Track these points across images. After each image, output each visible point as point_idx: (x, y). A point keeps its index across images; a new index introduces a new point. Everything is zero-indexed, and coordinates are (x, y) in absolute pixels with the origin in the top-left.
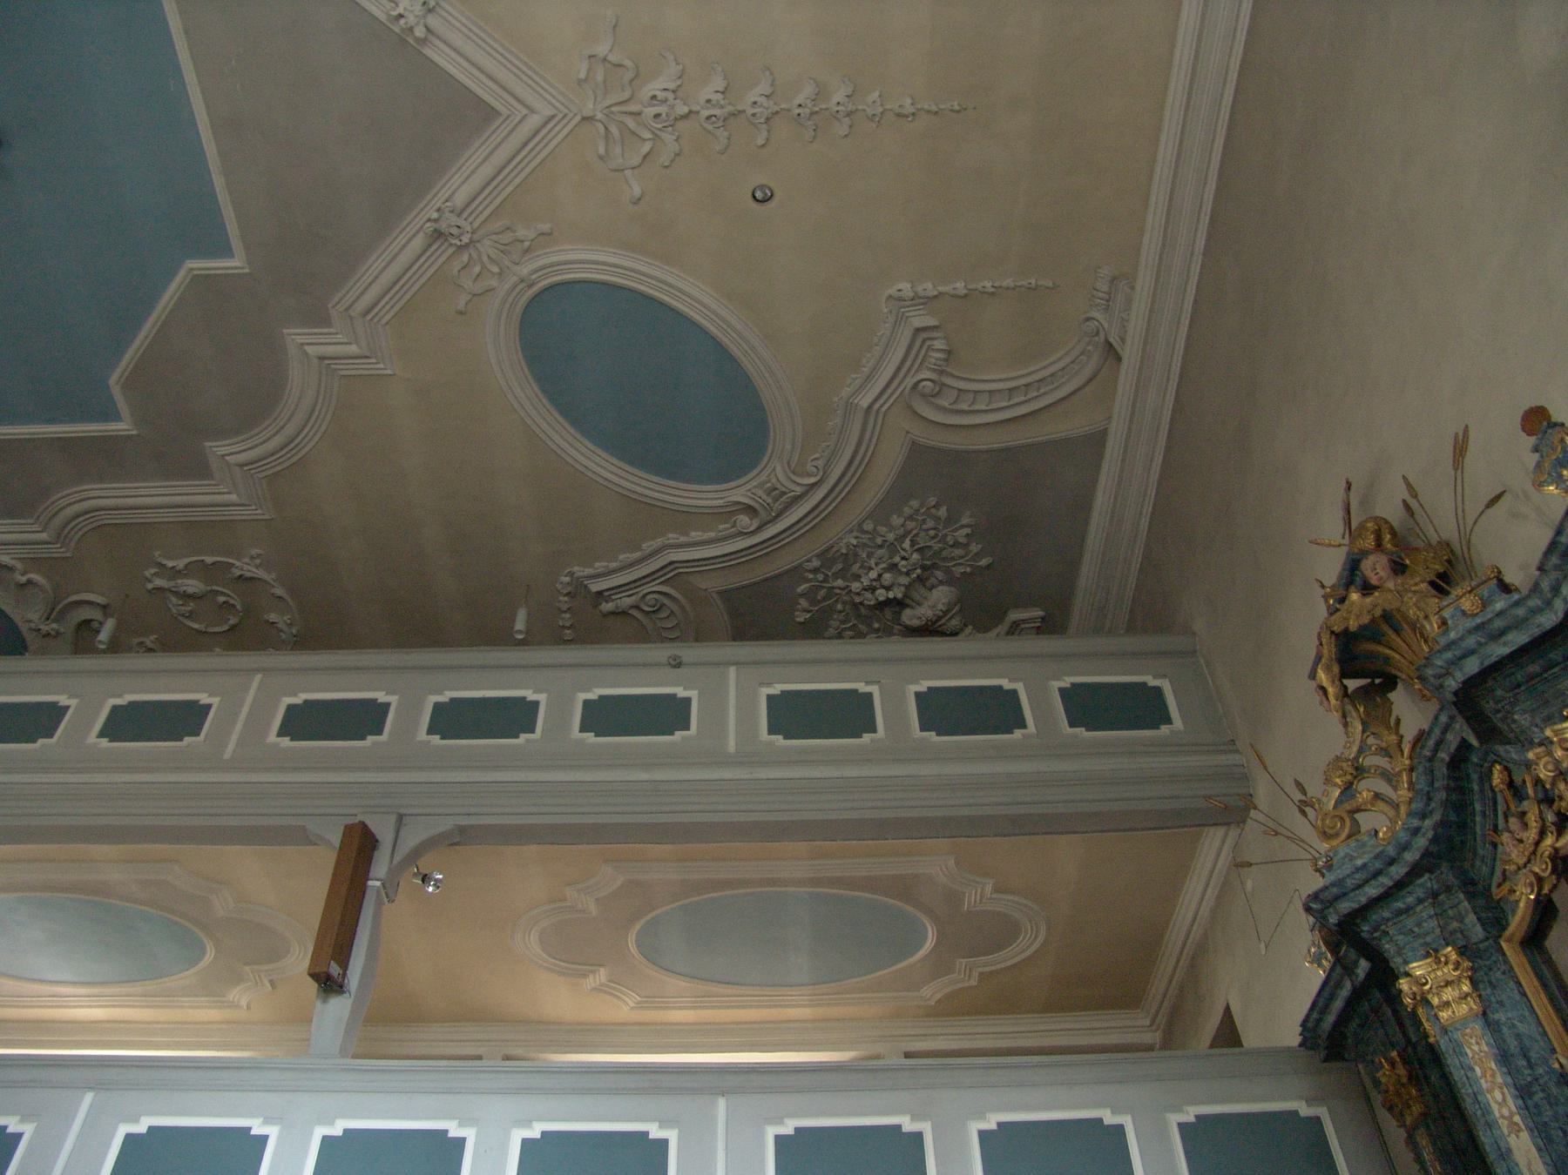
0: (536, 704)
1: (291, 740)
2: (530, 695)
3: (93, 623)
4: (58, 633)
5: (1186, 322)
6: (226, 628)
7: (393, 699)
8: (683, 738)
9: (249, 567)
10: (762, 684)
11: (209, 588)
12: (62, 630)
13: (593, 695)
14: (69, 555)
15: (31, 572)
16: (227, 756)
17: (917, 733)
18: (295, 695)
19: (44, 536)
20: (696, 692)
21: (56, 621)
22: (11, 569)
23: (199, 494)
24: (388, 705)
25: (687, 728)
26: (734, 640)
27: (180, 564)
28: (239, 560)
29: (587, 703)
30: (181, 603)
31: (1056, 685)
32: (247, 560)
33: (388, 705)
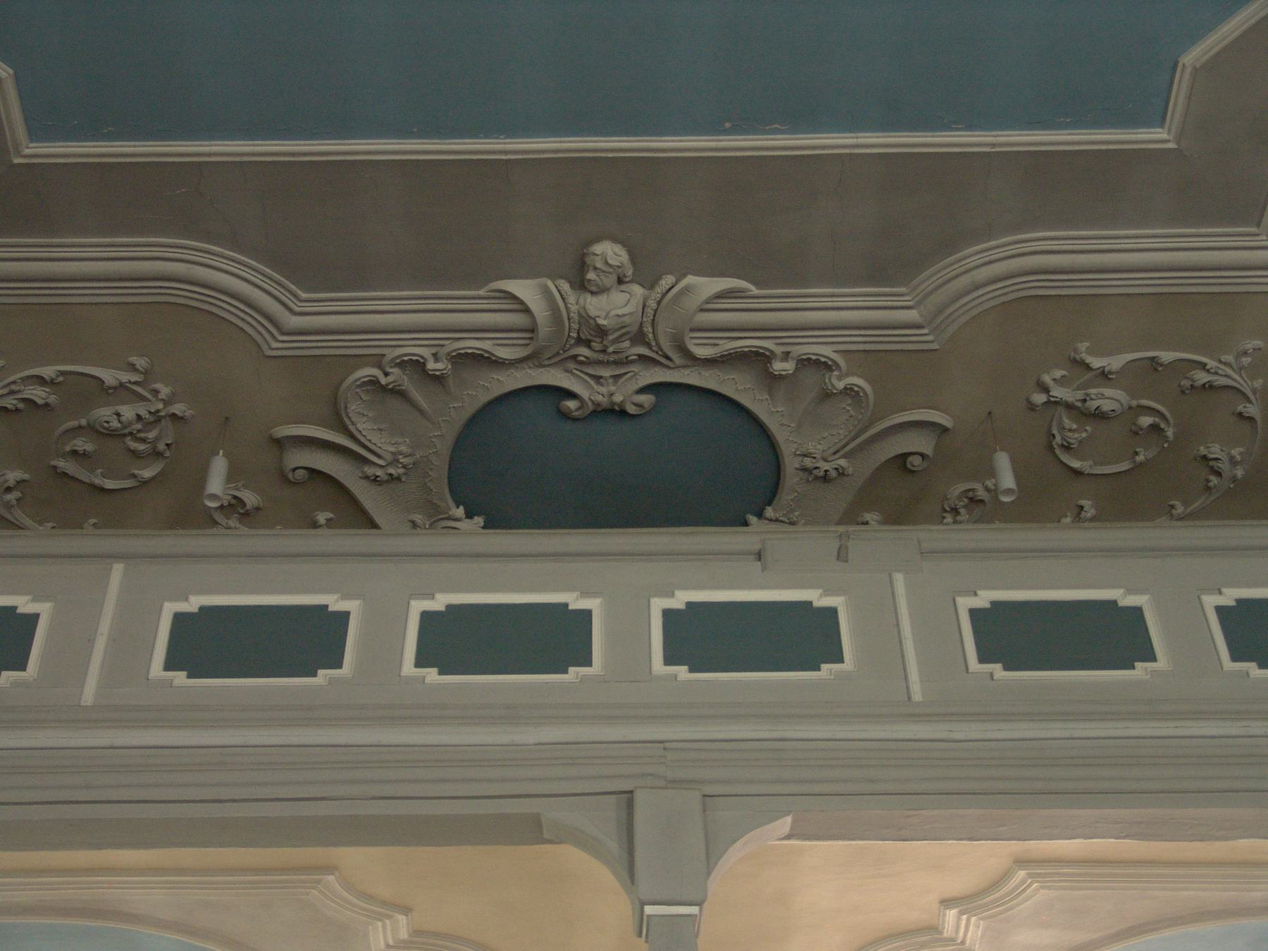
0: (32, 620)
1: (189, 677)
2: (335, 603)
3: (910, 459)
4: (841, 473)
5: (1176, 81)
6: (1124, 466)
7: (44, 609)
8: (332, 681)
9: (1230, 372)
10: (413, 596)
11: (1134, 403)
12: (850, 471)
13: (439, 603)
14: (935, 346)
15: (853, 374)
16: (89, 695)
17: (1228, 664)
18: (432, 596)
19: (912, 315)
20: (413, 603)
21: (845, 456)
22: (825, 366)
23: (227, 272)
24: (35, 618)
25: (588, 662)
26: (171, 527)
27: (1115, 363)
28: (1212, 358)
29: (426, 617)
30: (1075, 426)
31: (965, 603)
32: (1229, 358)
33: (35, 618)
